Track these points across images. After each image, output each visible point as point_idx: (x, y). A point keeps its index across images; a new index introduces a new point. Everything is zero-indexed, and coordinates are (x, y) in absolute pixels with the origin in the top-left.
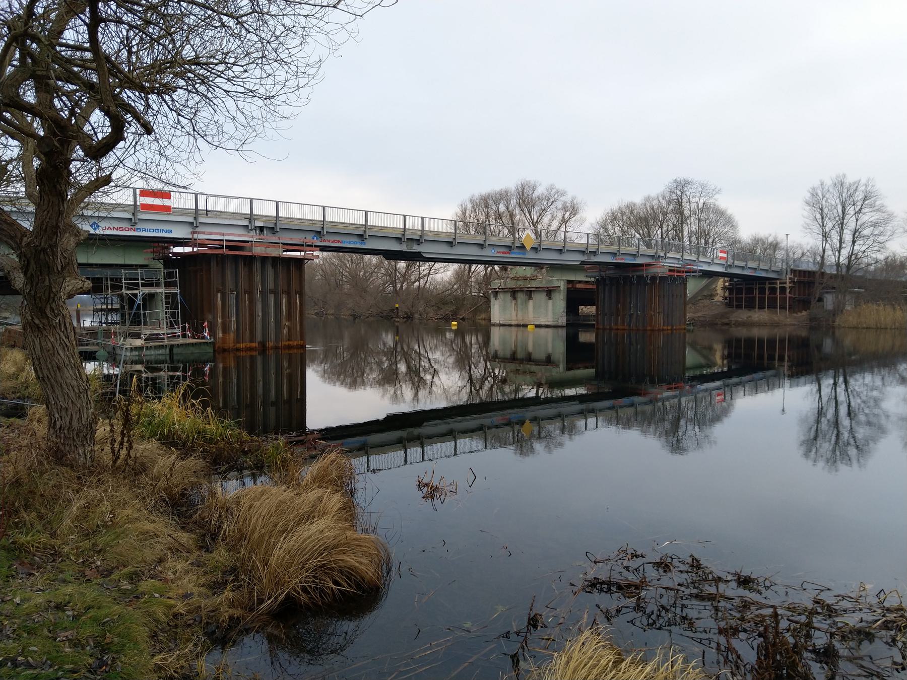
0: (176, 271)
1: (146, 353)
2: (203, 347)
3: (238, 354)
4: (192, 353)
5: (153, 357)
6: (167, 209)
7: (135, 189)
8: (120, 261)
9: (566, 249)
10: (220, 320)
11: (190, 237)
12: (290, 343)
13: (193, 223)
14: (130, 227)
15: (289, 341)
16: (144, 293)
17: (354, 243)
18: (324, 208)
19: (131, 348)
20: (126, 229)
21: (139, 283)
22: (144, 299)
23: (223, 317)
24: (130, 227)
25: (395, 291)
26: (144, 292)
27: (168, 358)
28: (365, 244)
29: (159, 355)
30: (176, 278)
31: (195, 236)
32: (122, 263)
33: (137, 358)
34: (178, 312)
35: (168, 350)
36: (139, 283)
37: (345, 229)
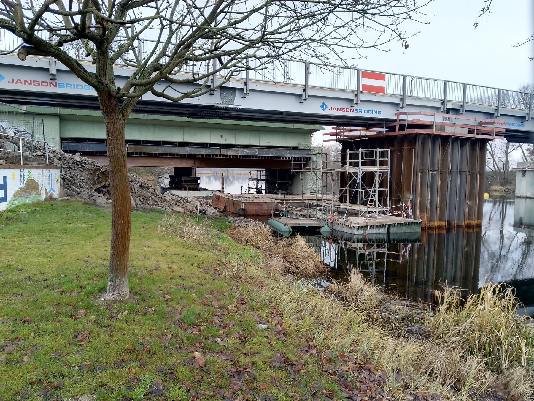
0: (388, 151)
1: (369, 232)
2: (413, 226)
3: (431, 232)
4: (405, 233)
5: (374, 236)
6: (381, 90)
7: (359, 71)
8: (151, 138)
9: (500, 112)
10: (419, 199)
11: (395, 117)
12: (471, 222)
13: (243, 89)
14: (350, 108)
15: (469, 219)
16: (363, 172)
17: (35, 82)
18: (445, 83)
19: (359, 227)
20: (348, 110)
21: (349, 162)
22: (363, 178)
23: (421, 198)
24: (350, 108)
25: (182, 181)
26: (363, 171)
27: (386, 237)
28: (523, 126)
29: (379, 234)
30: (388, 158)
31: (402, 117)
32: (91, 137)
33: (362, 237)
34: (387, 190)
35: (386, 229)
36: (349, 162)
37: (512, 112)
